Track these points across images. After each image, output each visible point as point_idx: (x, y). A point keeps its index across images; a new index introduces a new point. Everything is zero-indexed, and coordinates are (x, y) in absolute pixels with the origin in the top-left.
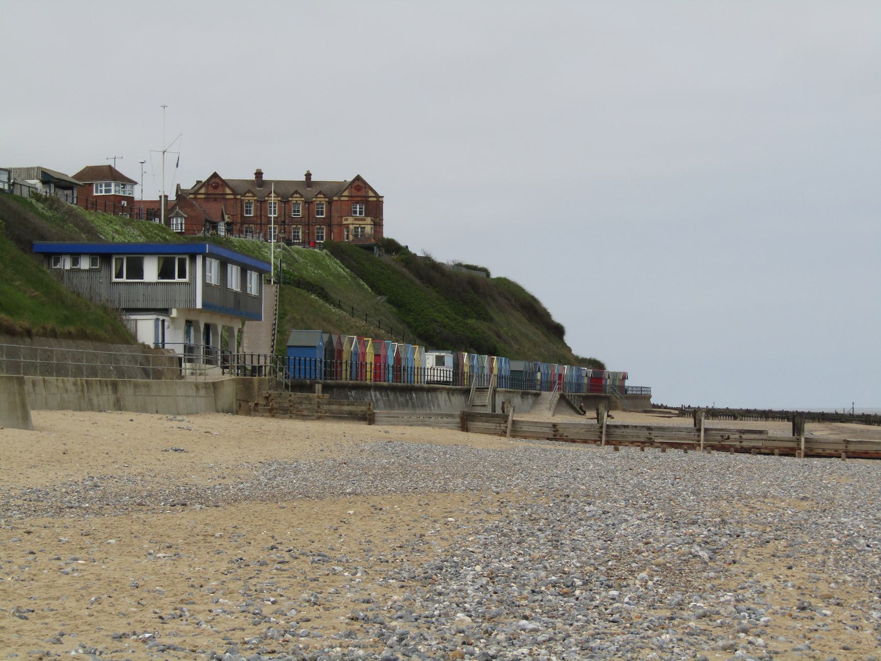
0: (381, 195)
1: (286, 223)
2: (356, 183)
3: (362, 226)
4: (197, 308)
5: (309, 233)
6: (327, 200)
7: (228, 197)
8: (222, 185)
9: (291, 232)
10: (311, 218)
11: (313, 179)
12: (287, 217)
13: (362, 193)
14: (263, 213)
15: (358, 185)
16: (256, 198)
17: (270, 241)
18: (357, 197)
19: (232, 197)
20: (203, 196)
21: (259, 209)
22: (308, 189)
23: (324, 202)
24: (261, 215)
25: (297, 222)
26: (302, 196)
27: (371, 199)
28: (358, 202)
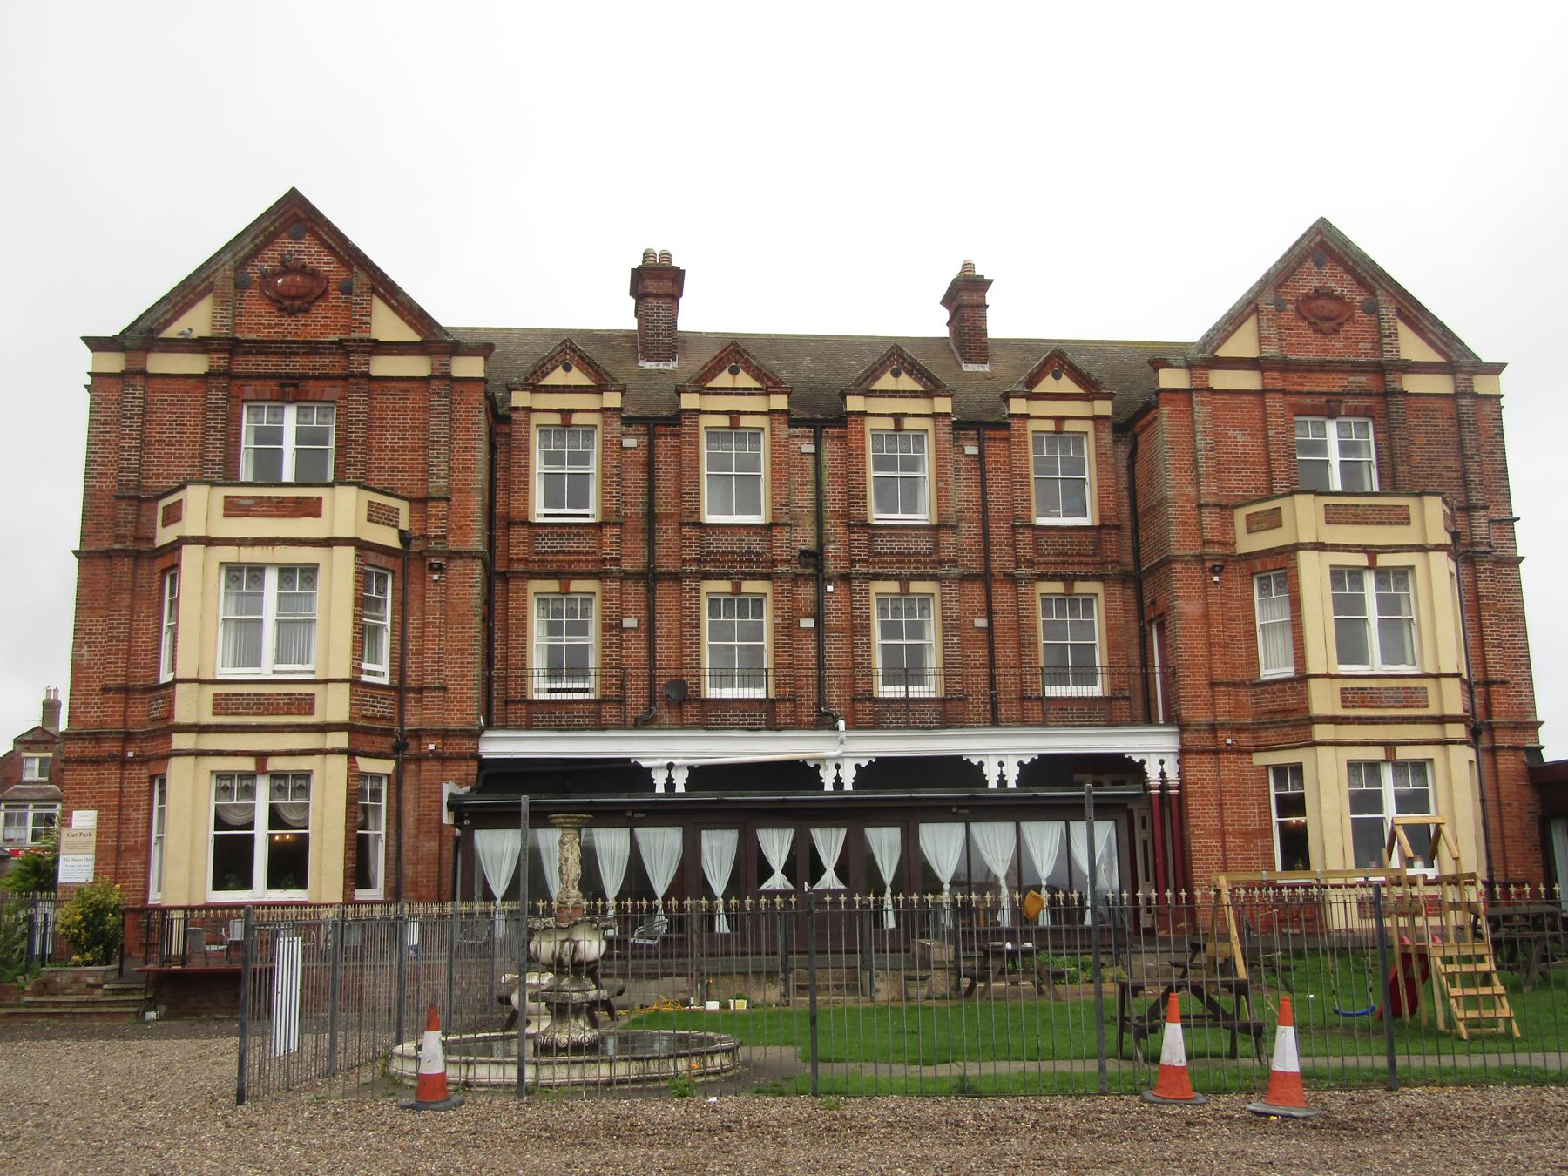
0: (1487, 357)
1: (831, 567)
2: (1311, 279)
3: (1384, 560)
4: (813, 626)
5: (990, 630)
6: (1104, 408)
7: (383, 366)
8: (347, 290)
9: (866, 629)
10: (999, 533)
11: (1002, 323)
12: (833, 526)
13: (1350, 346)
14: (665, 503)
15: (1320, 294)
16: (613, 399)
17: (237, 931)
18: (1323, 367)
19: (417, 366)
20: (196, 364)
21: (635, 475)
22: (968, 368)
23: (1087, 426)
24: (651, 517)
25: (902, 557)
26: (933, 388)
27: (1414, 384)
28: (1329, 407)
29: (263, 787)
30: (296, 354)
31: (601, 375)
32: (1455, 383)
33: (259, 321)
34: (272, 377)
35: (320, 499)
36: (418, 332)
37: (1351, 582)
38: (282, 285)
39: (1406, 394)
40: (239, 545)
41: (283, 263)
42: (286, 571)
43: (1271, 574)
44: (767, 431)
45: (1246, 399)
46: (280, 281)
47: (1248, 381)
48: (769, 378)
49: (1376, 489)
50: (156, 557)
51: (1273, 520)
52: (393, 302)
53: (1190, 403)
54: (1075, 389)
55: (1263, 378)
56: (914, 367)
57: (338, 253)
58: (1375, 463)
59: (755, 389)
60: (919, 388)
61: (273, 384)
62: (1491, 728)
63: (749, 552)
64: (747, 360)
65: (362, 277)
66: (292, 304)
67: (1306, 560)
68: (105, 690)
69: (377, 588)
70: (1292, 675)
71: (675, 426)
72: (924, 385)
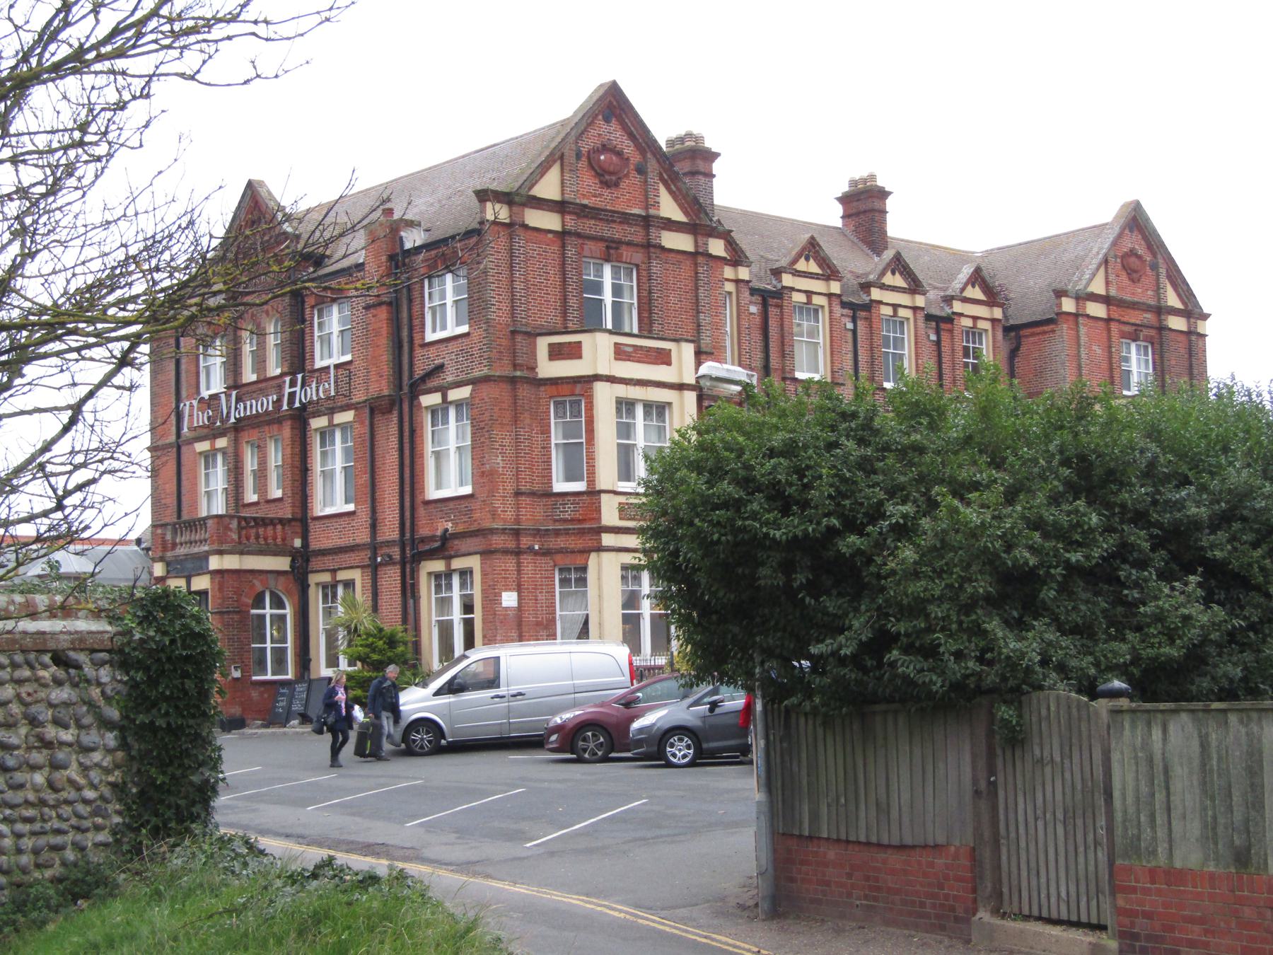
8: (641, 170)
29: (456, 581)
30: (614, 222)
31: (736, 253)
32: (563, 222)
33: (587, 190)
34: (602, 239)
35: (580, 342)
36: (686, 213)
37: (657, 415)
38: (605, 161)
39: (663, 249)
40: (627, 384)
41: (604, 146)
42: (648, 406)
43: (567, 399)
44: (827, 309)
45: (550, 236)
46: (602, 157)
47: (549, 221)
48: (829, 267)
49: (635, 331)
50: (541, 385)
51: (574, 352)
52: (673, 187)
53: (1077, 324)
54: (981, 296)
55: (1108, 310)
56: (905, 269)
57: (637, 139)
58: (636, 305)
59: (818, 274)
60: (904, 285)
61: (602, 245)
62: (374, 547)
64: (817, 252)
66: (607, 178)
67: (602, 390)
69: (571, 413)
71: (778, 298)
72: (909, 284)
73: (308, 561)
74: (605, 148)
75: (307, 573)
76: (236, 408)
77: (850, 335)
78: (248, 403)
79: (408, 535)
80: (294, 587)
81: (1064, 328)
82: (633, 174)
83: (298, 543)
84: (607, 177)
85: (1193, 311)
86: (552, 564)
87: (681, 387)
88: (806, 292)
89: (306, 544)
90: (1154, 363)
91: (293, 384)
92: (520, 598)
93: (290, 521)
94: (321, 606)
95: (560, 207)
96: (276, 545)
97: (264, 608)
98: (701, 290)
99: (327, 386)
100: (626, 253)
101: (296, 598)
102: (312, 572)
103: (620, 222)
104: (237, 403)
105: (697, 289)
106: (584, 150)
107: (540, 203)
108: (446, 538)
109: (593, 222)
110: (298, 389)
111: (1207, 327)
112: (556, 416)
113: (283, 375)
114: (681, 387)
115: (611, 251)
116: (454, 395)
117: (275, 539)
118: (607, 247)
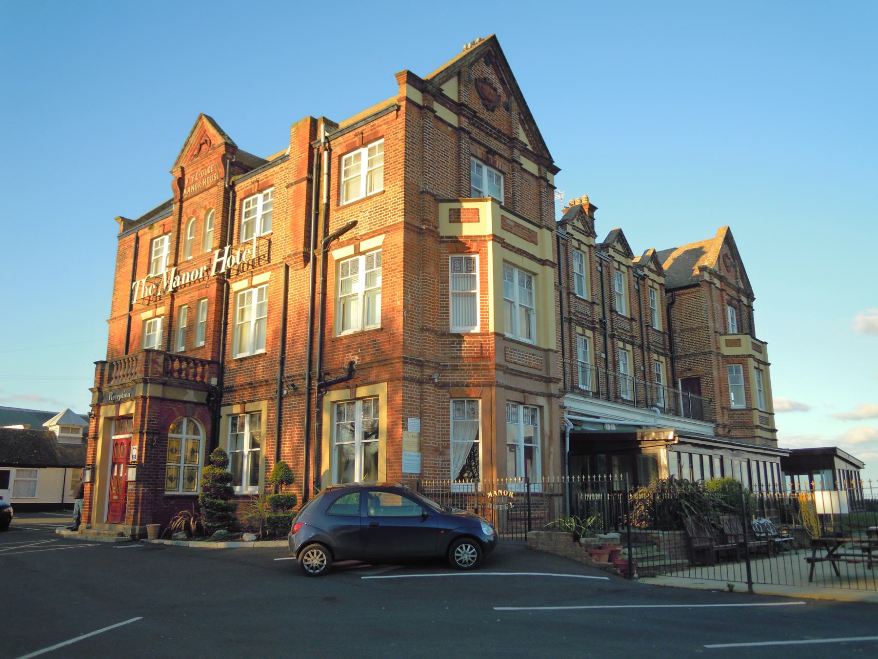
8: (508, 108)
30: (491, 136)
45: (450, 129)
53: (710, 287)
63: (586, 315)
65: (514, 106)
68: (423, 330)
70: (745, 408)
73: (221, 396)
74: (485, 80)
75: (220, 406)
76: (174, 280)
77: (599, 274)
78: (184, 275)
79: (316, 368)
80: (208, 417)
81: (704, 289)
82: (502, 109)
83: (214, 381)
84: (487, 103)
85: (750, 296)
86: (448, 396)
87: (543, 262)
88: (578, 240)
89: (221, 382)
90: (737, 320)
91: (221, 255)
92: (423, 425)
93: (209, 362)
94: (230, 433)
95: (458, 108)
96: (195, 380)
97: (181, 433)
98: (544, 204)
99: (249, 252)
100: (499, 163)
101: (209, 427)
102: (224, 405)
103: (495, 139)
104: (175, 275)
105: (541, 203)
106: (473, 77)
107: (445, 101)
108: (351, 370)
109: (478, 130)
110: (224, 258)
111: (755, 304)
112: (454, 270)
113: (214, 249)
114: (543, 262)
115: (489, 157)
116: (364, 246)
117: (195, 375)
118: (487, 152)
